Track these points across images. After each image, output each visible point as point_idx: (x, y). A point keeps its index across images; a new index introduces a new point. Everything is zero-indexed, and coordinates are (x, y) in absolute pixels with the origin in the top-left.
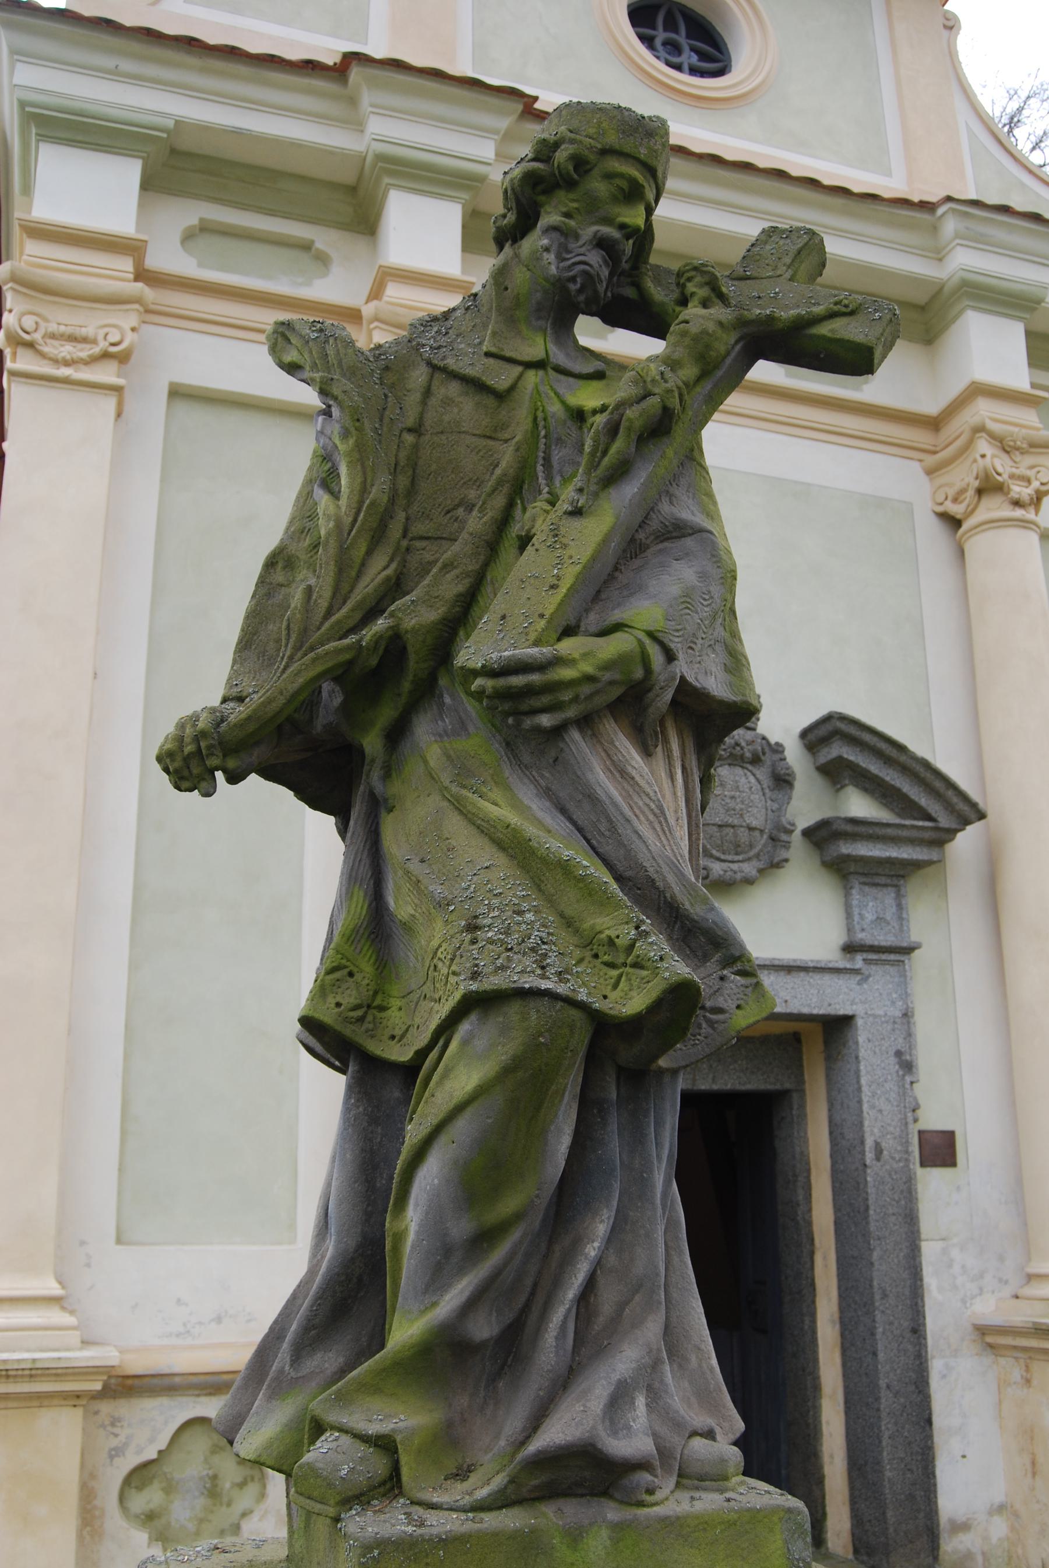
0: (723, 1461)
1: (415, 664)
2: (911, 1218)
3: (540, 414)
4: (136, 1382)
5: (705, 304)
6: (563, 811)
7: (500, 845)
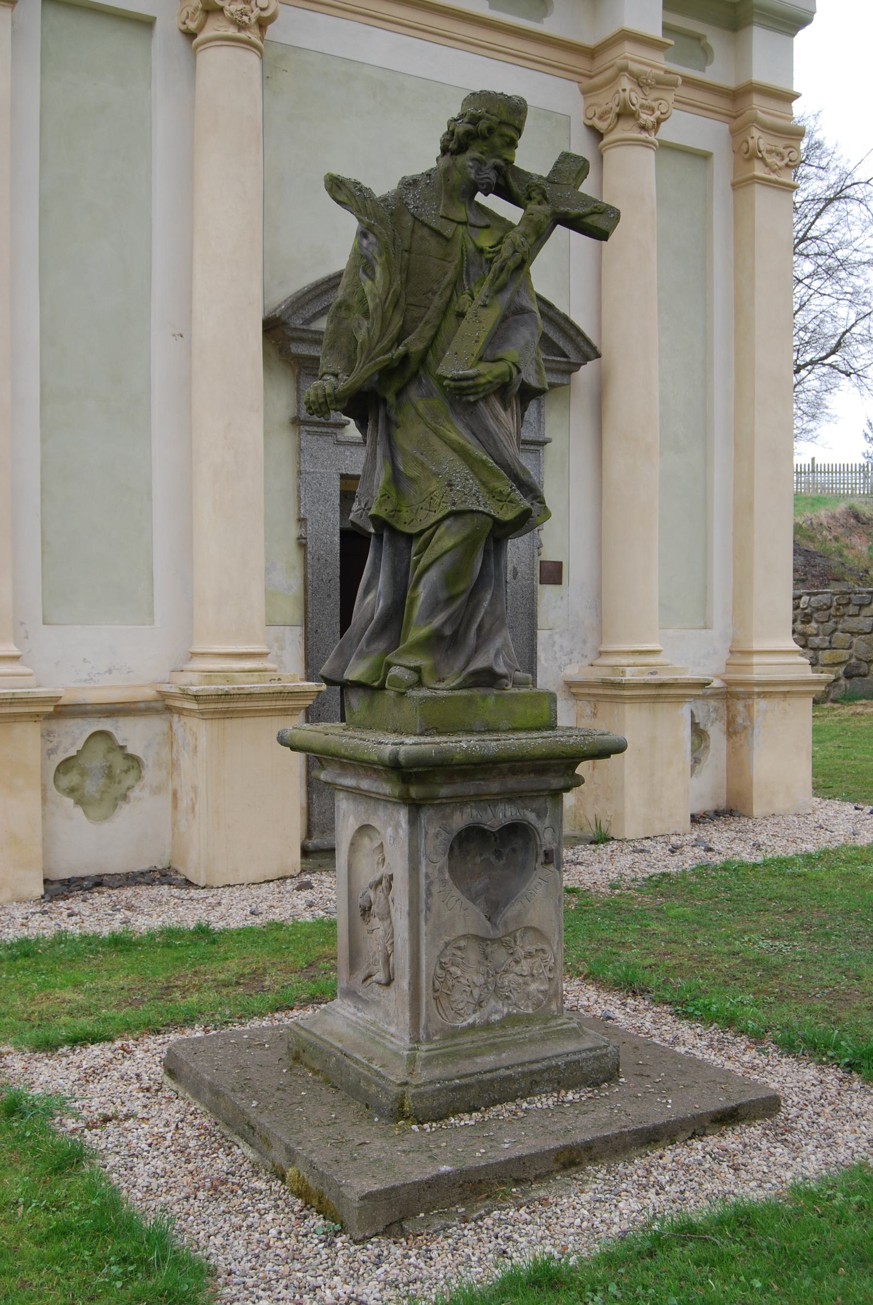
0: (528, 678)
1: (413, 365)
2: (532, 616)
3: (464, 249)
4: (64, 709)
5: (539, 203)
6: (474, 434)
7: (455, 450)
